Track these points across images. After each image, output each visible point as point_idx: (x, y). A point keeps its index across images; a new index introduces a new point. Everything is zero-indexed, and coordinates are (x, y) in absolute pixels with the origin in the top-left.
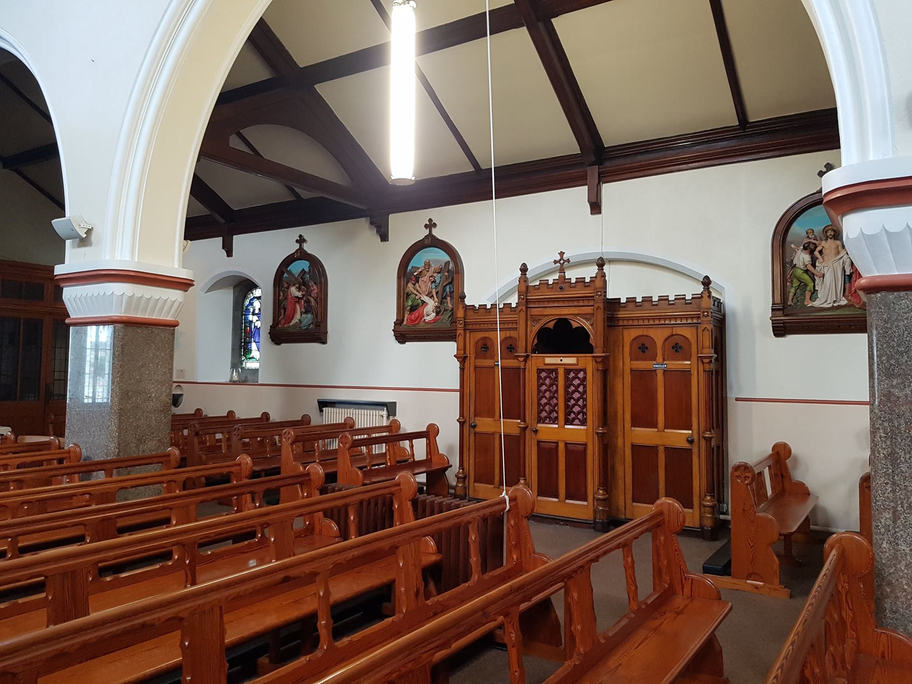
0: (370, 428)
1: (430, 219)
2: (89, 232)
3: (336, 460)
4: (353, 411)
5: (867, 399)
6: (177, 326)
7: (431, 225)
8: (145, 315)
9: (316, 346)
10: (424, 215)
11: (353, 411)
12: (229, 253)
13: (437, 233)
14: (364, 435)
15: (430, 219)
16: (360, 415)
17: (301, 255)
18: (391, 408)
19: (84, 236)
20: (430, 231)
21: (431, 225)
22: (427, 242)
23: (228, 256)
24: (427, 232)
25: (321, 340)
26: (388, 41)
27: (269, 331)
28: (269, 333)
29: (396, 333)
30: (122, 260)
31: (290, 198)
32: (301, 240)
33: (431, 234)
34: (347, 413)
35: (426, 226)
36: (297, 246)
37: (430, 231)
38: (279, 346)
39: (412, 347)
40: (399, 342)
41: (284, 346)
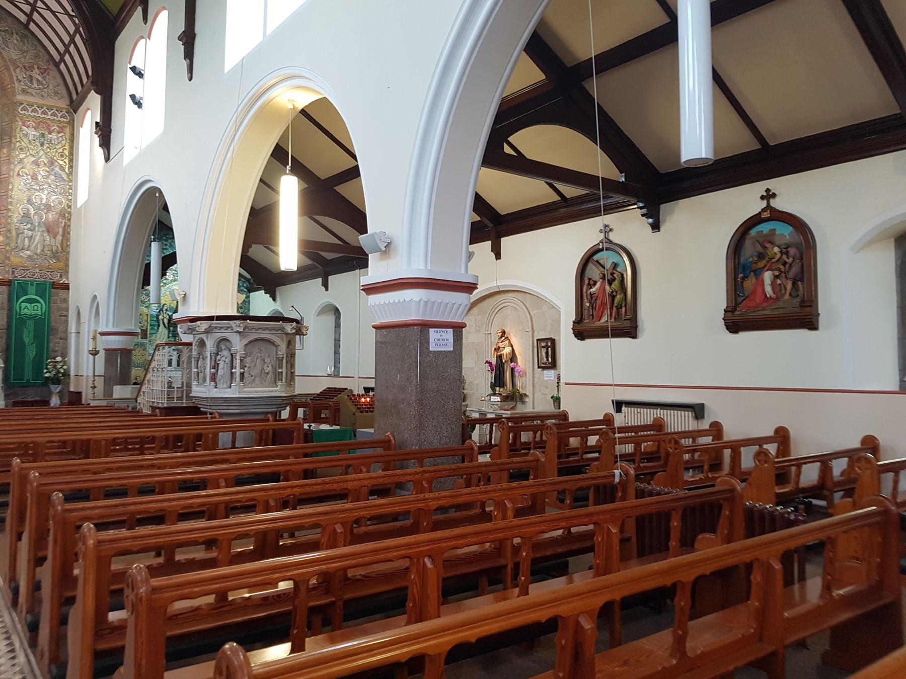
0: (638, 427)
1: (768, 189)
2: (389, 245)
3: (511, 448)
4: (660, 412)
5: (374, 376)
6: (465, 327)
7: (769, 195)
8: (448, 319)
9: (626, 341)
10: (759, 188)
11: (660, 412)
12: (498, 256)
13: (776, 203)
14: (628, 433)
15: (768, 189)
16: (687, 417)
17: (607, 245)
18: (698, 411)
19: (384, 249)
20: (768, 203)
21: (769, 195)
22: (766, 215)
23: (497, 259)
24: (764, 204)
25: (631, 334)
26: (274, 201)
27: (723, 317)
28: (723, 319)
29: (727, 321)
30: (417, 269)
31: (556, 198)
32: (607, 230)
33: (769, 206)
34: (654, 414)
35: (762, 198)
36: (602, 236)
37: (768, 203)
38: (583, 342)
39: (590, 342)
40: (730, 332)
41: (589, 341)
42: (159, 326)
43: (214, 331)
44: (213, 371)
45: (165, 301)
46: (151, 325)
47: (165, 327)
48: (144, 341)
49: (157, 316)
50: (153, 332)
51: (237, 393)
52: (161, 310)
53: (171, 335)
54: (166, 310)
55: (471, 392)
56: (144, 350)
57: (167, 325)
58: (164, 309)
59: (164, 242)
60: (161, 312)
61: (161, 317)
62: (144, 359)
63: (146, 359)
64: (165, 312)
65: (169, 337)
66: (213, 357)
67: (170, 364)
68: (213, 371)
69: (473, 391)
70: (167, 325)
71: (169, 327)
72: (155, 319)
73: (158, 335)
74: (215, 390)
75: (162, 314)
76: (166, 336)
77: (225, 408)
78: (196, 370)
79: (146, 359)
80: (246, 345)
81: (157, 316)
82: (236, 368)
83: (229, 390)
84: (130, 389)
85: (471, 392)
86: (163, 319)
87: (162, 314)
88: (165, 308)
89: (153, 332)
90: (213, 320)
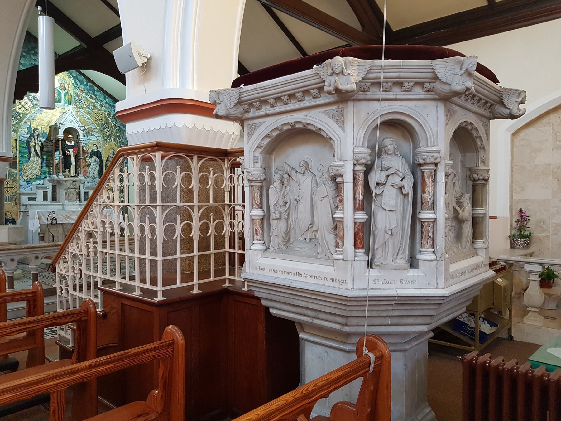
42: (30, 153)
43: (369, 95)
44: (362, 216)
45: (36, 125)
46: (20, 153)
47: (37, 155)
48: (13, 170)
49: (28, 143)
50: (24, 160)
51: (441, 282)
52: (32, 135)
53: (44, 165)
54: (38, 136)
55: (544, 234)
56: (13, 181)
57: (39, 153)
58: (35, 135)
59: (32, 56)
60: (32, 138)
61: (32, 144)
62: (14, 191)
63: (16, 192)
64: (36, 137)
65: (42, 167)
66: (361, 176)
67: (45, 197)
68: (362, 216)
69: (546, 233)
70: (39, 153)
71: (42, 155)
72: (25, 145)
73: (30, 165)
74: (373, 273)
75: (33, 140)
76: (39, 165)
77: (389, 321)
78: (258, 213)
79: (16, 192)
80: (515, 134)
81: (28, 143)
82: (433, 207)
83: (413, 272)
84: (7, 230)
85: (544, 234)
86: (35, 146)
87: (33, 140)
88: (36, 133)
89: (24, 160)
90: (380, 58)
